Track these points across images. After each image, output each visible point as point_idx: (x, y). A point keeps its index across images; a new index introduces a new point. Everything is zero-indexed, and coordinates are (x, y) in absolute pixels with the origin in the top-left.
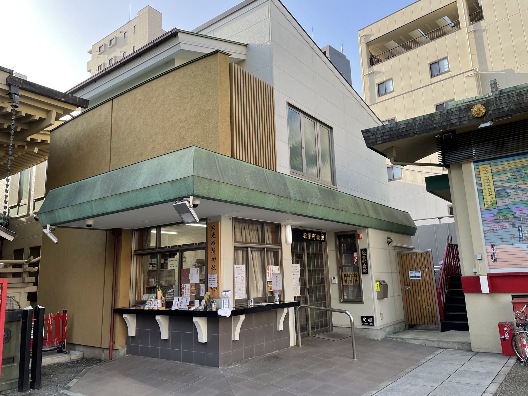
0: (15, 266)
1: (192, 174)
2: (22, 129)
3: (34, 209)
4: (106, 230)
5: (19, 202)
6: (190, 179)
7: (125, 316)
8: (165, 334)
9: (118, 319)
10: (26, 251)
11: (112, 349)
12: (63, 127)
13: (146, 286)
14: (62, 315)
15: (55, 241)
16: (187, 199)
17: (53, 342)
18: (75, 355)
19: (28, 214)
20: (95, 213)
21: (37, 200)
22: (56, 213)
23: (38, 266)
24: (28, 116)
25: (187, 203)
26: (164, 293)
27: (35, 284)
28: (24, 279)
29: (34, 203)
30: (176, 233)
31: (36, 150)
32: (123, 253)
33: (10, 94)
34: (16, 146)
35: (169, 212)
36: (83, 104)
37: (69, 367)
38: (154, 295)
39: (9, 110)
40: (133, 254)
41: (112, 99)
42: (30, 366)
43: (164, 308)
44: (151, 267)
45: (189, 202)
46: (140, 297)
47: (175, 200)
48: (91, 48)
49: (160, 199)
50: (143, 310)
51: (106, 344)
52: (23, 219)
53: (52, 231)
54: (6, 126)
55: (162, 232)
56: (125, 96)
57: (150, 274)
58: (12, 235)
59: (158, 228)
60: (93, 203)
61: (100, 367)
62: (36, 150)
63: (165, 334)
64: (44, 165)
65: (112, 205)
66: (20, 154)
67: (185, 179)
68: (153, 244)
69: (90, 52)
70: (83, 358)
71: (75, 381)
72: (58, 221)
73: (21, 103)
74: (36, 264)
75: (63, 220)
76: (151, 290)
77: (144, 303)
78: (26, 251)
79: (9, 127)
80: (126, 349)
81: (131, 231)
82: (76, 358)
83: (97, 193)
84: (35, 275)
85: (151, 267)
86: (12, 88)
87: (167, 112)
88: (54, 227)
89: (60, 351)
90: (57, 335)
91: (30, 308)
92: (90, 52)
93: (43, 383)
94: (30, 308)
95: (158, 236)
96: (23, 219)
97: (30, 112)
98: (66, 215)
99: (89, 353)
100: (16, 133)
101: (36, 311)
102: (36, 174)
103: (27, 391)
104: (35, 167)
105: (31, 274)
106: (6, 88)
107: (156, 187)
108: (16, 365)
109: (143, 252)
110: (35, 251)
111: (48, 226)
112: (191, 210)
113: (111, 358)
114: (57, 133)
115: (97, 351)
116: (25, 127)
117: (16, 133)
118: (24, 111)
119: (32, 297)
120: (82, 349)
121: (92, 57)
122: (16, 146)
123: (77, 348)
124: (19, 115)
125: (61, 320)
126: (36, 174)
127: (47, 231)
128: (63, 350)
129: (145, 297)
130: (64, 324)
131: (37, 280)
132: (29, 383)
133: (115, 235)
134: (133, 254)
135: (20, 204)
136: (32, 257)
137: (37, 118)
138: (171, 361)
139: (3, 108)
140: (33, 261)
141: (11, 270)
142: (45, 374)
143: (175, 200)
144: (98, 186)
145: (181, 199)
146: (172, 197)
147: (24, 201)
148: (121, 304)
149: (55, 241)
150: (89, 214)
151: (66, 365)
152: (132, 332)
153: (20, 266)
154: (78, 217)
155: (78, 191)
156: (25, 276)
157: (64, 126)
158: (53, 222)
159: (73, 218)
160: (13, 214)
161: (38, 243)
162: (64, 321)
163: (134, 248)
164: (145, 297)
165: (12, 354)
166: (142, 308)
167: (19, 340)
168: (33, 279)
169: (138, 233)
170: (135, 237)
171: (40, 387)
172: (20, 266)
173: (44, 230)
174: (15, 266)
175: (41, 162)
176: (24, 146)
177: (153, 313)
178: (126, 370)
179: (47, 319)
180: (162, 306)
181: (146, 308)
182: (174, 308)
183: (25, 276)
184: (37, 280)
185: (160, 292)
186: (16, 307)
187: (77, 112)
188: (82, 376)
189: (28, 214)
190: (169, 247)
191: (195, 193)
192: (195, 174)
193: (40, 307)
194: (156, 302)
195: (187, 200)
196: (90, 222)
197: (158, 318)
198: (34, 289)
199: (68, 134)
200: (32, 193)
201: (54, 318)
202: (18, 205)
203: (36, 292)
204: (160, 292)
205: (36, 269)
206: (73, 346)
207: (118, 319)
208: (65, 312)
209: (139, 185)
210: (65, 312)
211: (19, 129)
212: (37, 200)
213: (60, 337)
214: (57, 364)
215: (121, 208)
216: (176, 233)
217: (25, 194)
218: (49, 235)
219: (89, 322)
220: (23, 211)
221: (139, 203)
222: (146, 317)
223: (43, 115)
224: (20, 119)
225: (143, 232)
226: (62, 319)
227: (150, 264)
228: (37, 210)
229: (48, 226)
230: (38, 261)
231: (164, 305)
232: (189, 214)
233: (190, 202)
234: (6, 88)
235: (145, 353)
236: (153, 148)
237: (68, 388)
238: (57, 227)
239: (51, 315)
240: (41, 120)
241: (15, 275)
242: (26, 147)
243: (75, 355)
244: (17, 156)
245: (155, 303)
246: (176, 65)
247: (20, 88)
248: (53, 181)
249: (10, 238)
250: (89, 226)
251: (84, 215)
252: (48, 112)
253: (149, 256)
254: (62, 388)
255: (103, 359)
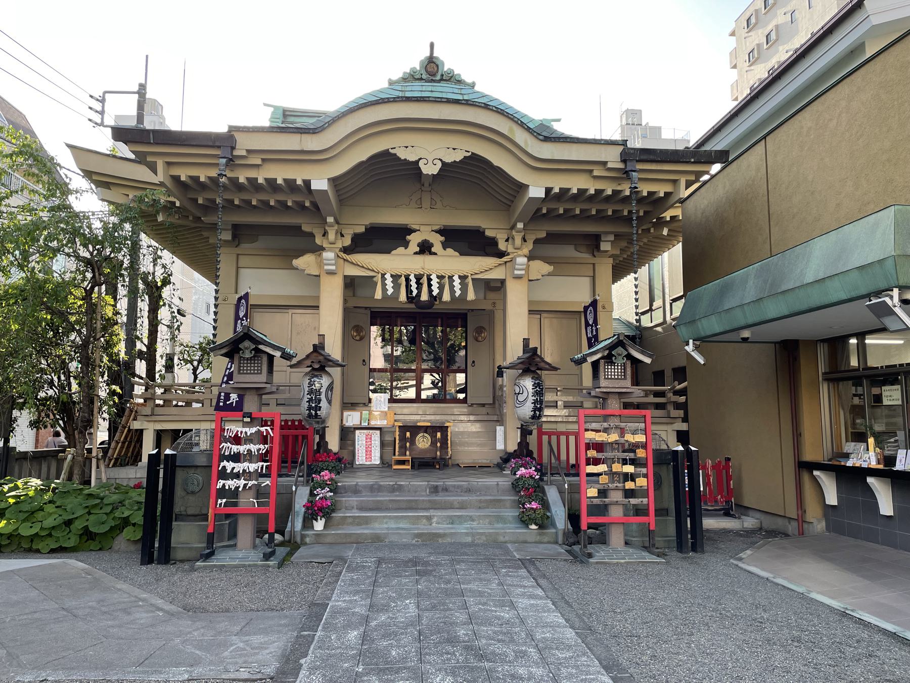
0: (657, 394)
1: (893, 253)
2: (645, 212)
3: (671, 314)
4: (775, 343)
5: (651, 305)
6: (890, 264)
7: (816, 473)
8: (886, 507)
9: (806, 477)
10: (669, 374)
11: (801, 520)
12: (698, 193)
13: (850, 430)
14: (723, 463)
15: (702, 362)
16: (890, 293)
17: (716, 501)
18: (749, 522)
19: (665, 322)
20: (750, 321)
21: (675, 300)
22: (699, 324)
23: (686, 395)
24: (651, 194)
25: (887, 300)
26: (878, 444)
27: (685, 419)
28: (669, 412)
29: (671, 304)
30: (902, 342)
31: (665, 232)
32: (805, 375)
33: (626, 172)
34: (640, 232)
35: (859, 314)
36: (722, 156)
37: (741, 535)
38: (863, 446)
39: (627, 193)
40: (821, 379)
41: (765, 137)
42: (689, 526)
43: (881, 467)
44: (856, 401)
45: (891, 297)
46: (840, 446)
47: (868, 296)
48: (732, 26)
49: (844, 297)
50: (845, 466)
51: (792, 512)
52: (659, 329)
53: (697, 348)
54: (626, 213)
55: (867, 341)
56: (785, 127)
57: (857, 411)
58: (650, 356)
59: (861, 336)
60: (745, 307)
61: (785, 542)
62: (665, 232)
63: (886, 507)
64: (677, 250)
65: (773, 309)
66: (645, 240)
67: (881, 262)
68: (854, 362)
69: (733, 34)
70: (761, 529)
71: (749, 552)
72: (703, 334)
73: (640, 179)
74: (682, 392)
75: (709, 333)
76: (860, 437)
77: (847, 456)
78: (669, 374)
79: (630, 212)
80: (824, 524)
81: (813, 344)
82: (751, 526)
83: (750, 294)
84: (683, 406)
85: (856, 401)
86: (628, 164)
87: (858, 139)
88: (698, 343)
89: (727, 513)
90: (720, 492)
91: (681, 448)
92: (733, 34)
93: (706, 548)
94: (681, 448)
95: (862, 349)
96: (659, 329)
97: (653, 188)
98: (712, 325)
99: (768, 523)
100: (638, 218)
101: (688, 452)
102: (669, 264)
103: (687, 553)
104: (666, 254)
105: (677, 406)
106: (621, 166)
107: (836, 277)
108: (672, 519)
109: (838, 375)
110: (680, 373)
111: (691, 341)
112: (898, 310)
113: (801, 533)
114: (690, 204)
115: (780, 521)
116: (648, 209)
117: (638, 218)
118: (645, 189)
119: (683, 437)
120: (758, 515)
121: (737, 41)
122: (640, 232)
123: (751, 513)
124: (640, 196)
125: (724, 471)
126: (669, 264)
127: (690, 348)
128: (732, 513)
129: (849, 447)
130: (729, 478)
131: (686, 414)
132: (690, 544)
133: (789, 353)
134: (821, 379)
135: (653, 308)
136: (676, 382)
137: (662, 195)
138: (901, 551)
139: (621, 191)
140: (678, 387)
141: (651, 399)
142: (709, 539)
143: (868, 296)
144: (751, 283)
145: (878, 294)
146: (864, 291)
147: (658, 303)
148: (809, 455)
149: (702, 362)
150: (742, 323)
151: (737, 534)
152: (832, 498)
153: (661, 394)
154: (728, 329)
155: (723, 292)
156: (670, 407)
157: (701, 197)
158: (696, 337)
159: (722, 330)
160: (646, 322)
161: (682, 363)
162: (728, 472)
163: (822, 368)
164: (849, 447)
165: (665, 505)
166: (843, 464)
167: (672, 484)
168: (681, 413)
169: (826, 345)
170: (822, 353)
171: (703, 552)
172: (661, 394)
173: (686, 348)
174: (657, 394)
175: (674, 246)
176: (649, 230)
177: (862, 473)
178: (822, 551)
179: (704, 468)
180: (879, 463)
181: (849, 463)
182: (899, 467)
183: (670, 407)
184: (686, 414)
185: (871, 441)
186: (664, 447)
187: (716, 168)
188: (759, 548)
189: (665, 322)
190: (882, 367)
191: (901, 283)
192: (898, 252)
193: (693, 449)
194: (867, 456)
195: (887, 296)
196: (746, 334)
197: (870, 480)
198: (684, 427)
199: (706, 202)
200: (667, 291)
201: (713, 467)
202: (651, 310)
203: (688, 432)
204: (871, 441)
205: (682, 399)
206: (744, 510)
207: (806, 477)
208: (728, 460)
209: (810, 278)
210: (728, 460)
211: (641, 214)
212: (675, 300)
213: (725, 493)
214: (724, 529)
215: (786, 313)
216: (902, 342)
217: (658, 293)
218: (693, 354)
219: (763, 475)
220: (658, 317)
221: (813, 305)
222: (853, 479)
223: (668, 188)
224: (641, 200)
225: (837, 344)
226: (723, 468)
227: (855, 395)
228: (677, 314)
229: (691, 341)
230: (686, 388)
231: (882, 461)
232: (894, 317)
233: (893, 299)
234: (621, 166)
235: (854, 533)
236: (838, 205)
237: (740, 559)
238: (702, 342)
239: (709, 463)
240: (668, 195)
241: (658, 406)
242: (652, 230)
243: (749, 522)
244: (642, 244)
245: (866, 456)
246: (868, 55)
247: (637, 161)
248: (693, 274)
249: (648, 360)
250: (745, 340)
251: (736, 325)
252: (675, 182)
253: (850, 382)
254: (731, 557)
255: (790, 533)
